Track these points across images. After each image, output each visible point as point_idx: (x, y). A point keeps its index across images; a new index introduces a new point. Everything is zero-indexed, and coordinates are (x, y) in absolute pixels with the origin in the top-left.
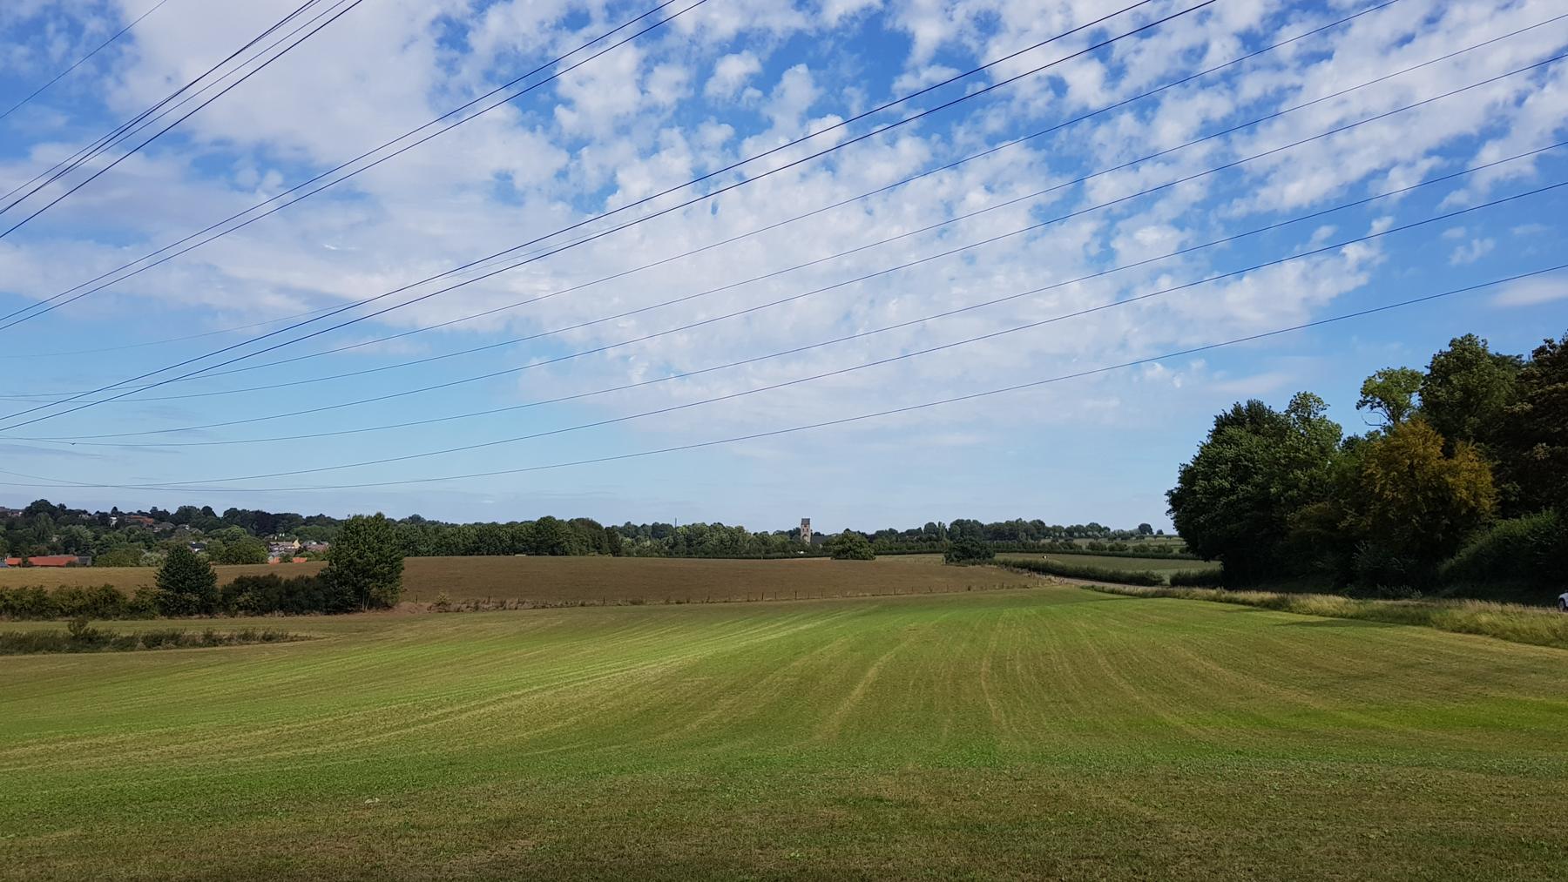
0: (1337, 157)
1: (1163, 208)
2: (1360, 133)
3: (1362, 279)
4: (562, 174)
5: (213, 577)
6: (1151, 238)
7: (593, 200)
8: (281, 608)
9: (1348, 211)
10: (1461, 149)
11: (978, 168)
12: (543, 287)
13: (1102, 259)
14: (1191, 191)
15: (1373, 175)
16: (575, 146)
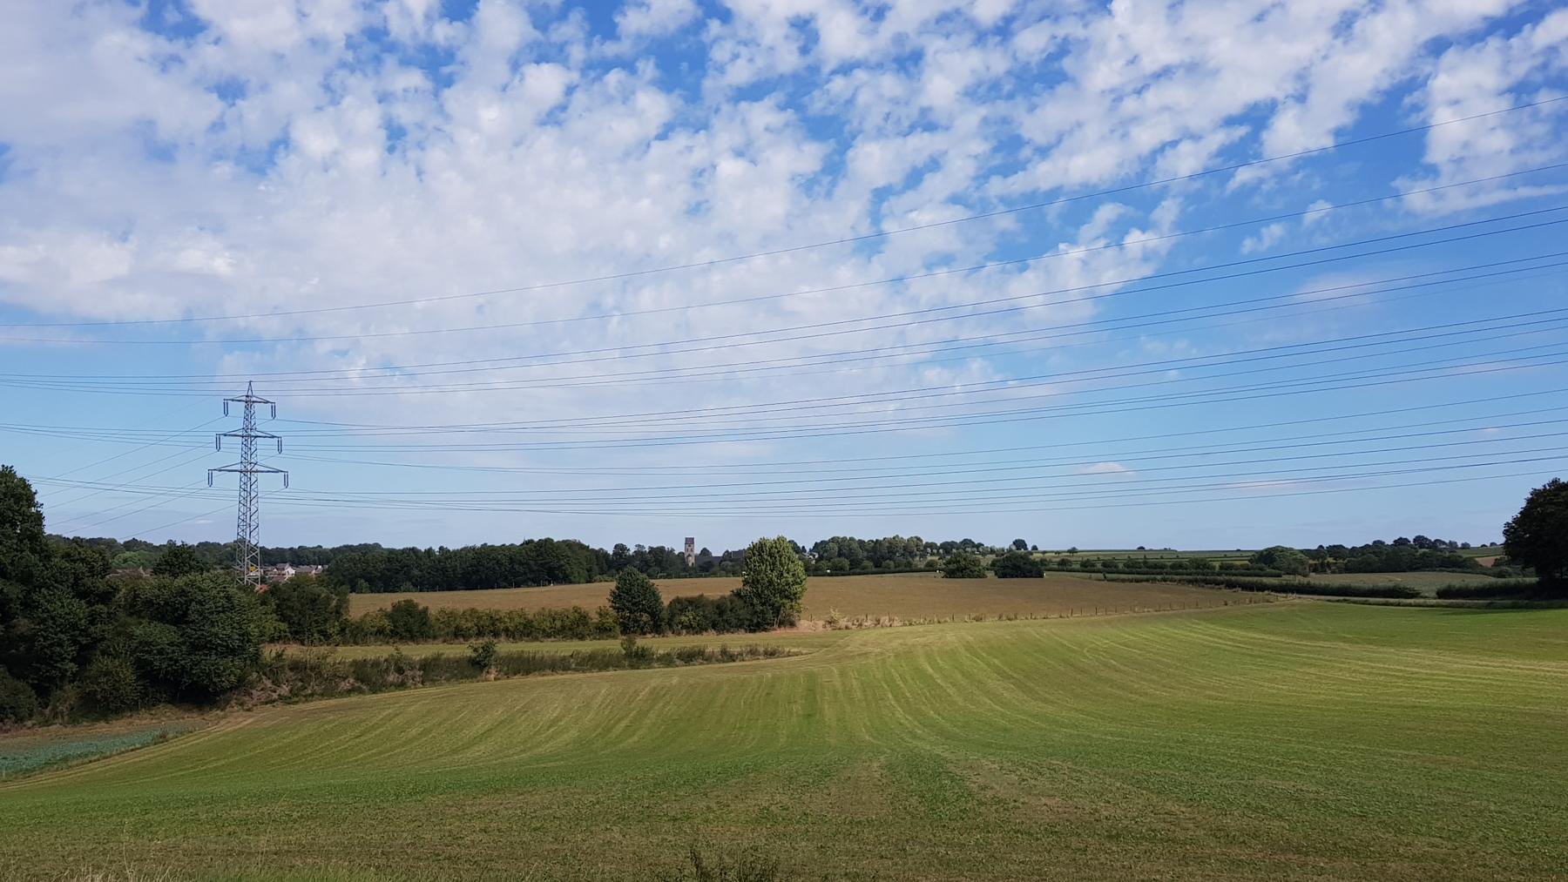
0: (1122, 129)
1: (935, 185)
2: (1152, 98)
3: (1147, 270)
4: (218, 126)
5: (655, 596)
6: (927, 223)
7: (264, 157)
8: (714, 627)
9: (1135, 193)
10: (1258, 117)
11: (726, 136)
12: (222, 265)
13: (870, 245)
14: (959, 170)
15: (1162, 149)
16: (230, 90)
